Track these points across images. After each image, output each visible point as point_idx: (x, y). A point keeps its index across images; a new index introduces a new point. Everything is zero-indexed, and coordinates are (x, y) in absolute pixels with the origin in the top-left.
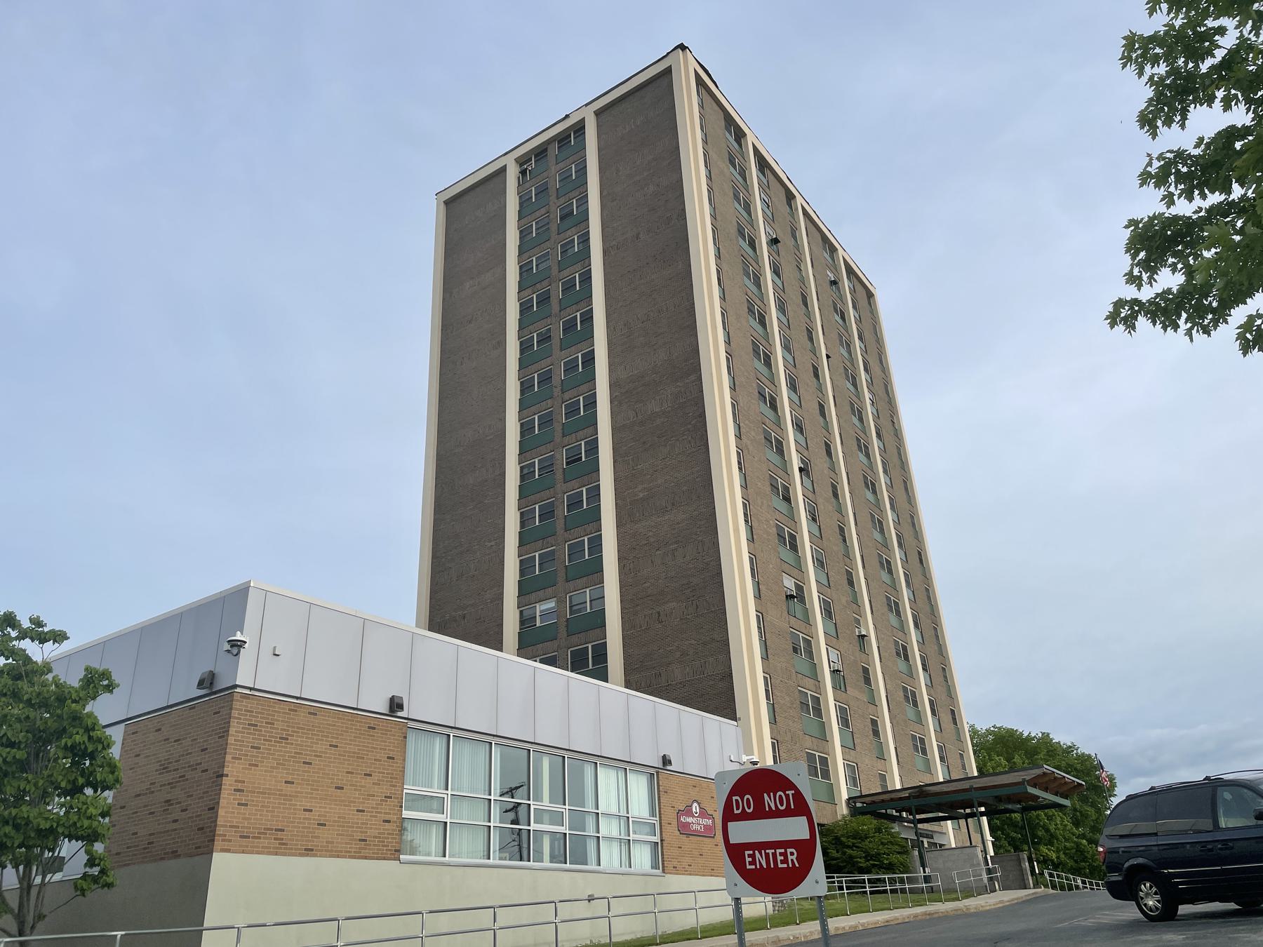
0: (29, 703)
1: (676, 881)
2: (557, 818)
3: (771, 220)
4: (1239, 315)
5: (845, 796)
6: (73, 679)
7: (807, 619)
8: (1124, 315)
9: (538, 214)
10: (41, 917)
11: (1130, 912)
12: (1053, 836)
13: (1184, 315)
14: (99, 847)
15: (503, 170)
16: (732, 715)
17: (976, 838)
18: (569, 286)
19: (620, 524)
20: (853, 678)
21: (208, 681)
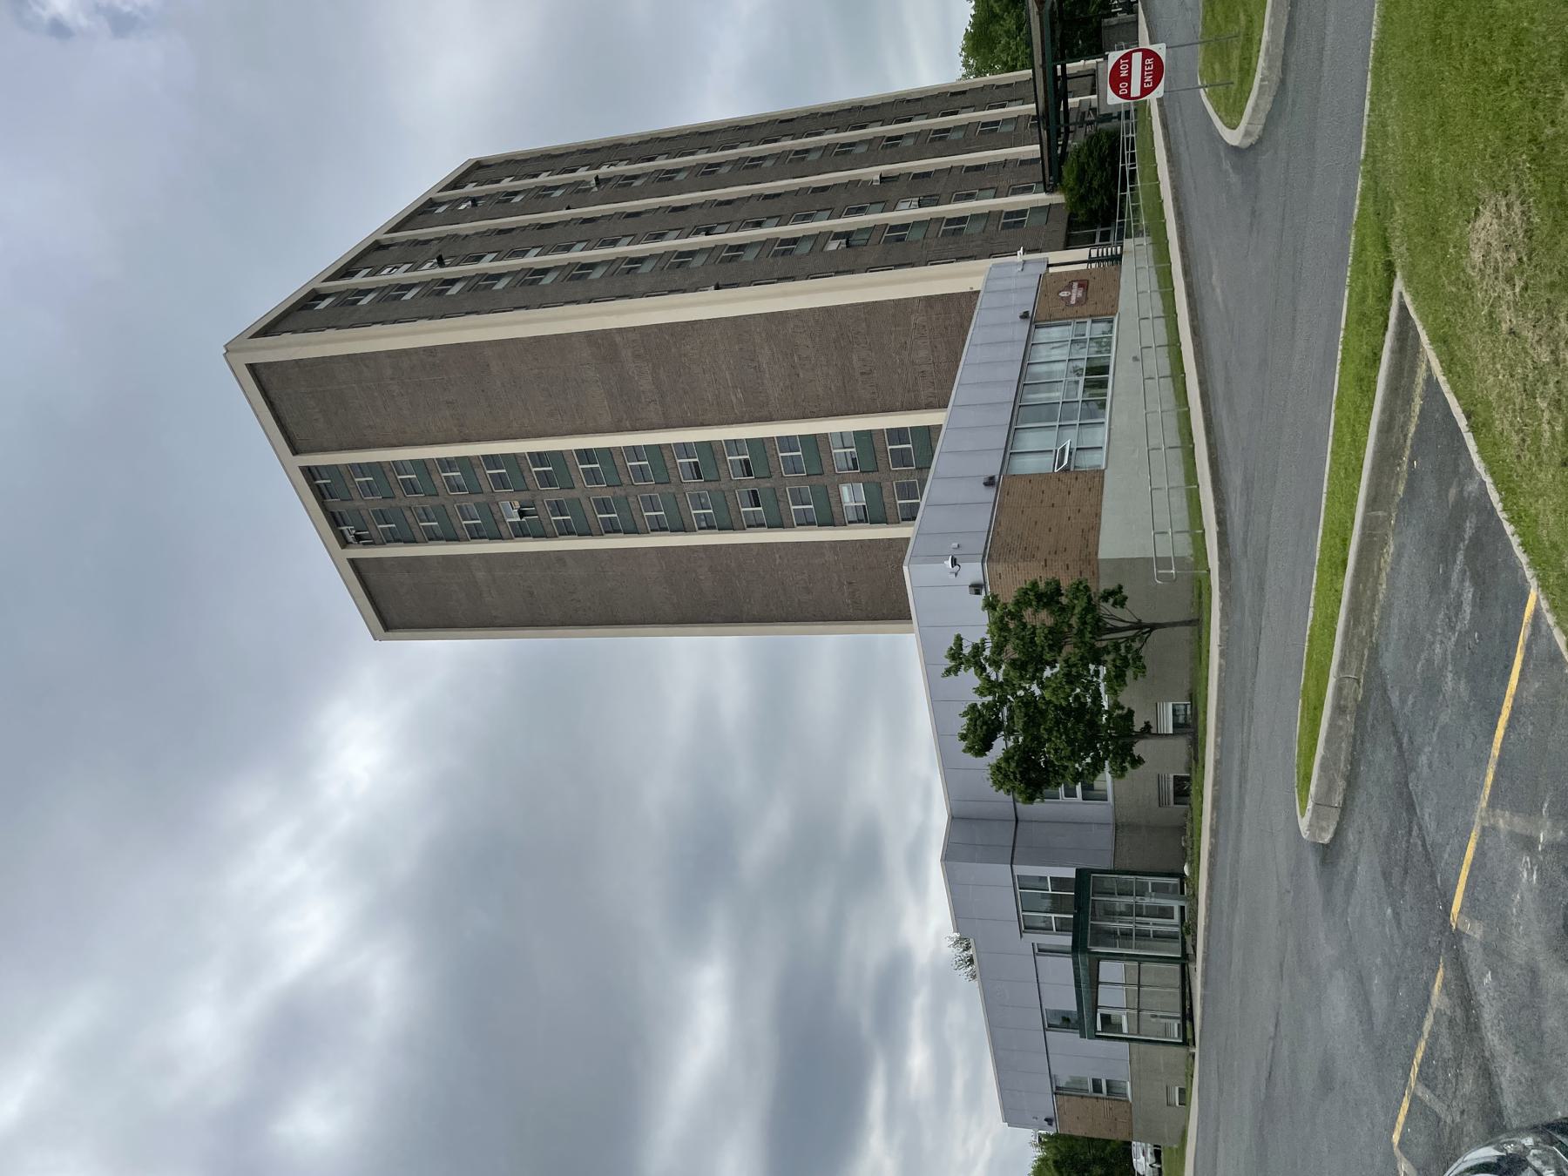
5: (1043, 196)
9: (411, 520)
15: (352, 562)
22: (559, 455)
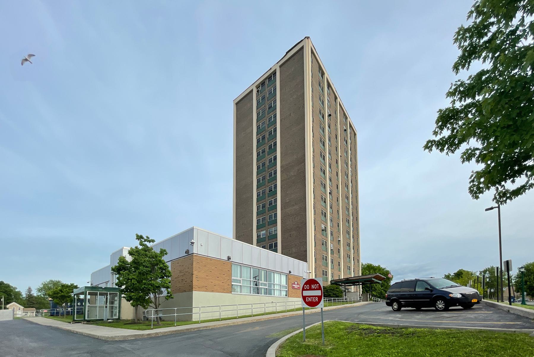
0: (149, 257)
1: (291, 299)
2: (265, 285)
3: (329, 107)
4: (464, 147)
6: (158, 251)
7: (326, 236)
8: (429, 146)
9: (262, 107)
10: (160, 304)
11: (390, 308)
12: (376, 289)
13: (447, 146)
14: (169, 290)
15: (252, 91)
16: (306, 261)
17: (358, 290)
18: (270, 133)
19: (282, 222)
20: (336, 251)
21: (187, 252)
22: (275, 150)
